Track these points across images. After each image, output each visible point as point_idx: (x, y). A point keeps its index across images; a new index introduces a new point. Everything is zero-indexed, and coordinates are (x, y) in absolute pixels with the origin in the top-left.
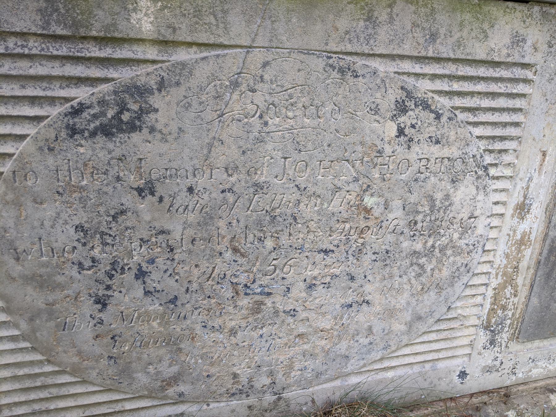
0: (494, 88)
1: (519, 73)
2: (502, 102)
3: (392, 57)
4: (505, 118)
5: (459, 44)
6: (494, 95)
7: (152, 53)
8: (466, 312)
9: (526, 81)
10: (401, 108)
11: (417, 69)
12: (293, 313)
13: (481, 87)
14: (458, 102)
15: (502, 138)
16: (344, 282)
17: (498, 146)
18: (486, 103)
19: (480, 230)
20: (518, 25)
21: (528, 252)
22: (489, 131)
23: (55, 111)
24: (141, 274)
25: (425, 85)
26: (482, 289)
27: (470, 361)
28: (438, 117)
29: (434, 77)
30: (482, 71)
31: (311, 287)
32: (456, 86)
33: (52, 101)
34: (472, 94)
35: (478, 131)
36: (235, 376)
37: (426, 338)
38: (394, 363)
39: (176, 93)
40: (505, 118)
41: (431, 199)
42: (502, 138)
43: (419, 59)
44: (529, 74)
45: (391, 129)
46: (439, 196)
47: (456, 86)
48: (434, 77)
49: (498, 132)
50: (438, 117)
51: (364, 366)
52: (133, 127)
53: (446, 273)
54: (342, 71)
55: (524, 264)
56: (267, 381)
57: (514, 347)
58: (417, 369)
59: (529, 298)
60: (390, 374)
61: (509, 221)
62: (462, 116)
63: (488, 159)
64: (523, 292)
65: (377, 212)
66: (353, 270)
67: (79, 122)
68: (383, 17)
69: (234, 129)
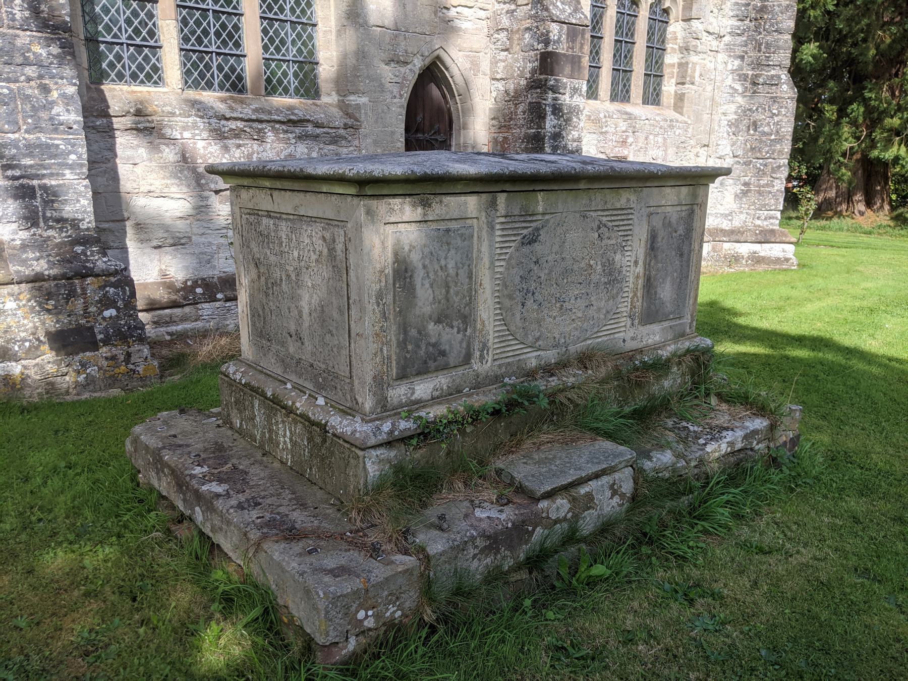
0: (623, 217)
1: (630, 211)
2: (625, 222)
3: (595, 211)
4: (627, 228)
5: (613, 204)
6: (623, 220)
7: (540, 217)
8: (623, 310)
9: (632, 214)
10: (599, 228)
11: (602, 214)
12: (571, 310)
13: (619, 218)
14: (614, 224)
15: (627, 235)
16: (585, 296)
17: (626, 238)
18: (621, 223)
19: (624, 273)
20: (628, 195)
21: (640, 281)
22: (623, 233)
23: (519, 238)
24: (533, 294)
25: (604, 219)
26: (626, 299)
27: (727, 172)
28: (609, 229)
29: (607, 216)
30: (619, 212)
31: (576, 298)
32: (613, 218)
33: (518, 234)
34: (617, 220)
35: (620, 233)
36: (555, 338)
37: (605, 328)
38: (601, 334)
39: (546, 228)
40: (627, 228)
41: (609, 260)
42: (627, 235)
43: (603, 210)
44: (632, 211)
45: (596, 235)
46: (611, 259)
47: (613, 218)
48: (607, 216)
49: (625, 233)
50: (609, 229)
51: (592, 335)
52: (536, 241)
53: (615, 291)
54: (584, 217)
55: (639, 287)
56: (563, 341)
57: (641, 328)
58: (608, 337)
59: (643, 303)
60: (600, 340)
61: (632, 268)
62: (615, 228)
63: (624, 244)
64: (640, 300)
65: (594, 267)
66: (588, 291)
67: (525, 241)
68: (593, 199)
69: (558, 239)
